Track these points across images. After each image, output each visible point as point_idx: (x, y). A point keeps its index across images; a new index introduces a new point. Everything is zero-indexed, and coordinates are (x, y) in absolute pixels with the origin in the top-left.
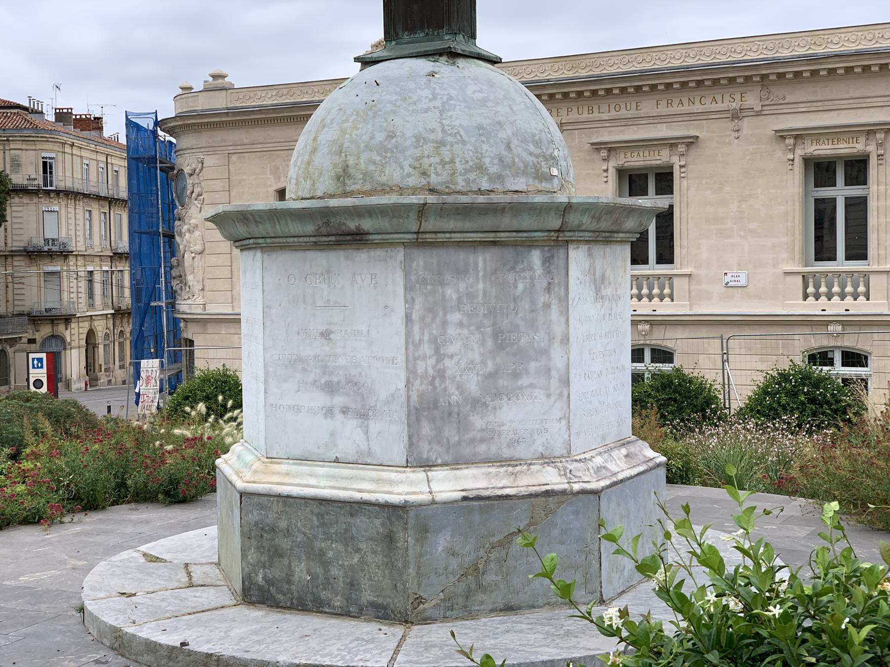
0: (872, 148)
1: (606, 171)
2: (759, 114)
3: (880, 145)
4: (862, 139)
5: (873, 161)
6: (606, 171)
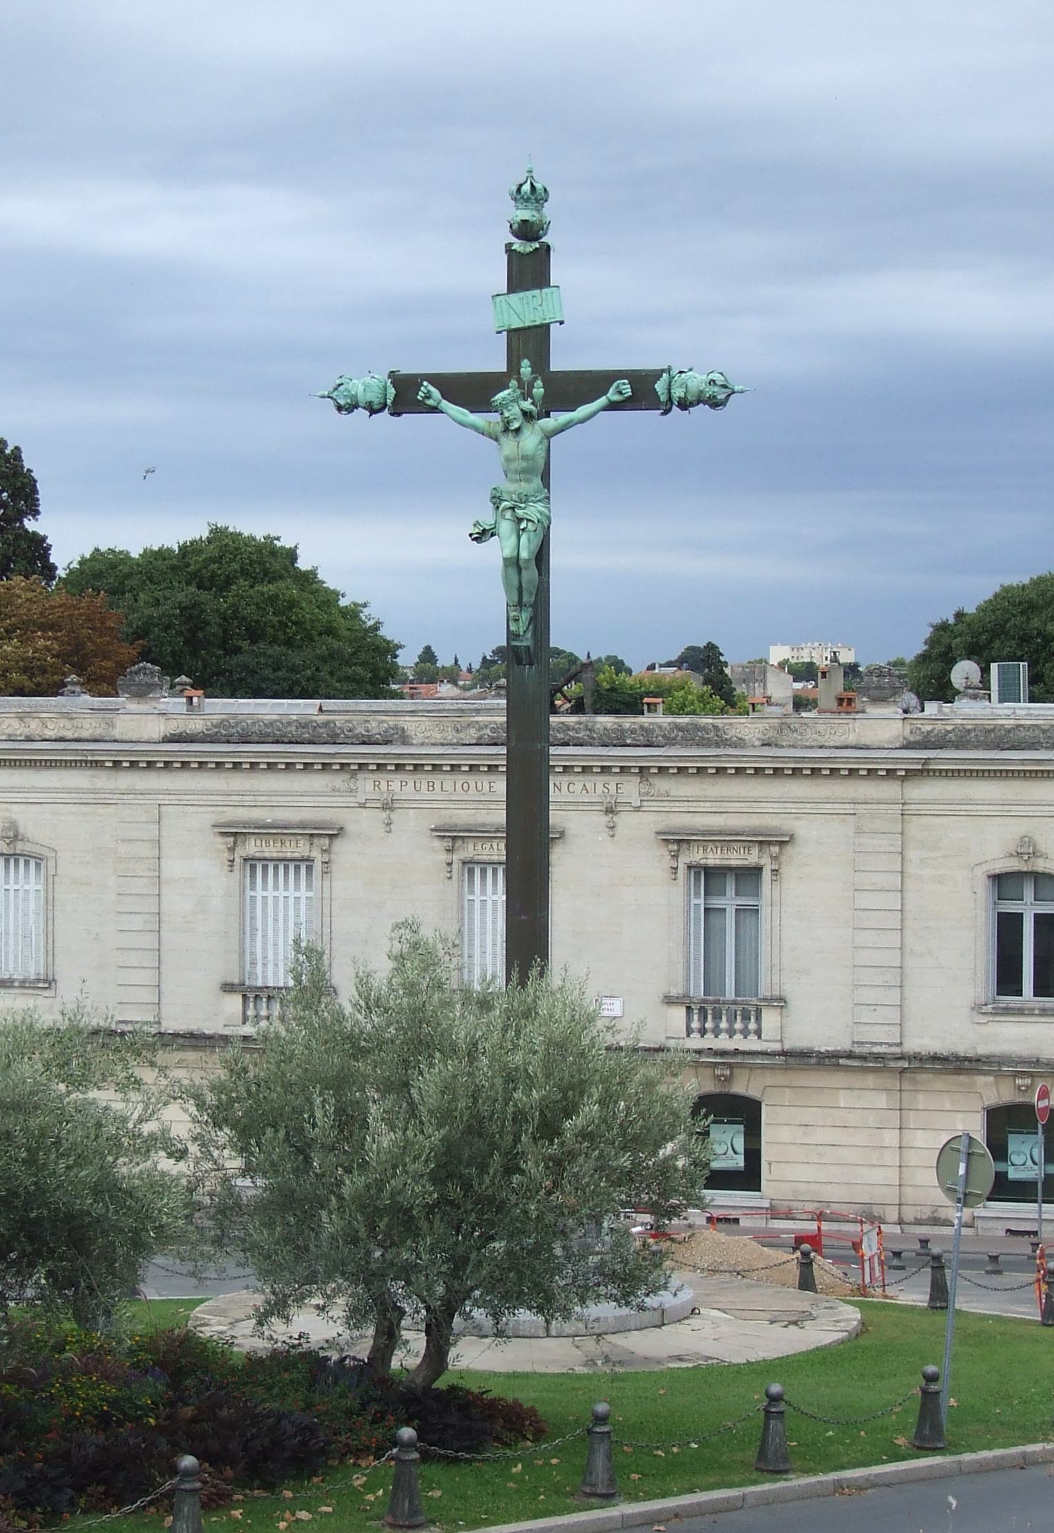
0: (765, 861)
1: (450, 864)
2: (638, 809)
3: (775, 858)
4: (755, 851)
5: (766, 875)
6: (450, 864)
